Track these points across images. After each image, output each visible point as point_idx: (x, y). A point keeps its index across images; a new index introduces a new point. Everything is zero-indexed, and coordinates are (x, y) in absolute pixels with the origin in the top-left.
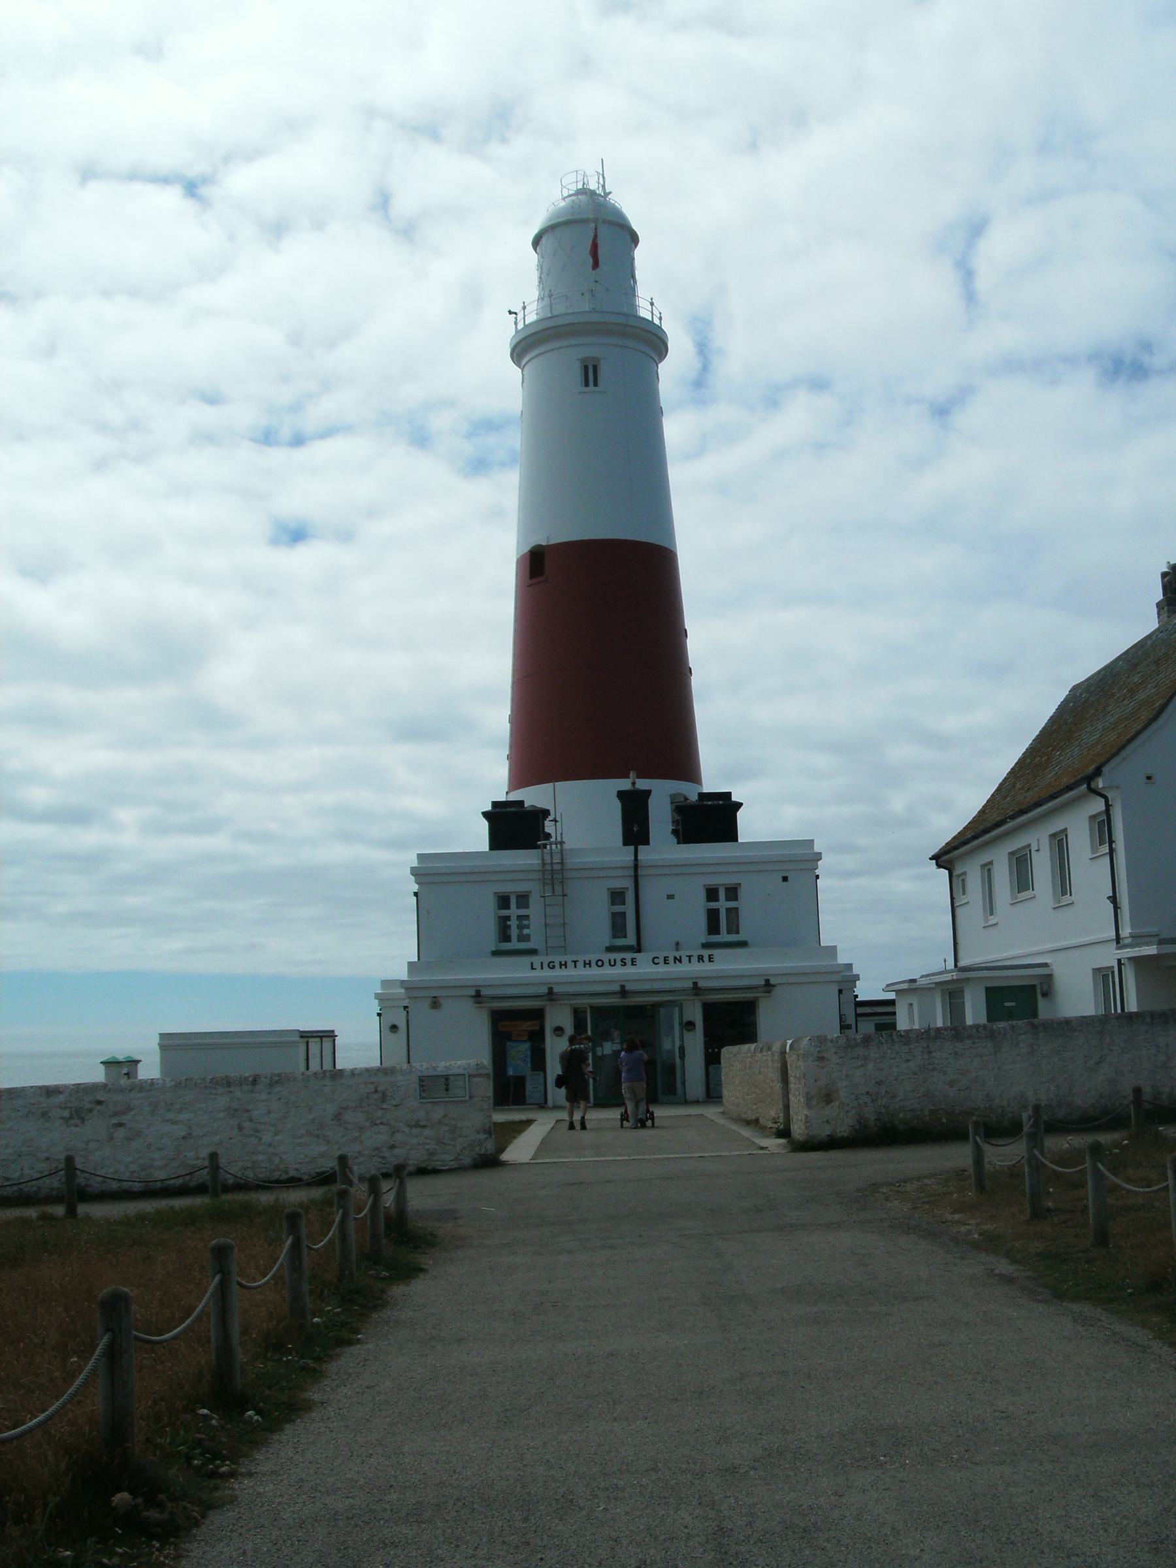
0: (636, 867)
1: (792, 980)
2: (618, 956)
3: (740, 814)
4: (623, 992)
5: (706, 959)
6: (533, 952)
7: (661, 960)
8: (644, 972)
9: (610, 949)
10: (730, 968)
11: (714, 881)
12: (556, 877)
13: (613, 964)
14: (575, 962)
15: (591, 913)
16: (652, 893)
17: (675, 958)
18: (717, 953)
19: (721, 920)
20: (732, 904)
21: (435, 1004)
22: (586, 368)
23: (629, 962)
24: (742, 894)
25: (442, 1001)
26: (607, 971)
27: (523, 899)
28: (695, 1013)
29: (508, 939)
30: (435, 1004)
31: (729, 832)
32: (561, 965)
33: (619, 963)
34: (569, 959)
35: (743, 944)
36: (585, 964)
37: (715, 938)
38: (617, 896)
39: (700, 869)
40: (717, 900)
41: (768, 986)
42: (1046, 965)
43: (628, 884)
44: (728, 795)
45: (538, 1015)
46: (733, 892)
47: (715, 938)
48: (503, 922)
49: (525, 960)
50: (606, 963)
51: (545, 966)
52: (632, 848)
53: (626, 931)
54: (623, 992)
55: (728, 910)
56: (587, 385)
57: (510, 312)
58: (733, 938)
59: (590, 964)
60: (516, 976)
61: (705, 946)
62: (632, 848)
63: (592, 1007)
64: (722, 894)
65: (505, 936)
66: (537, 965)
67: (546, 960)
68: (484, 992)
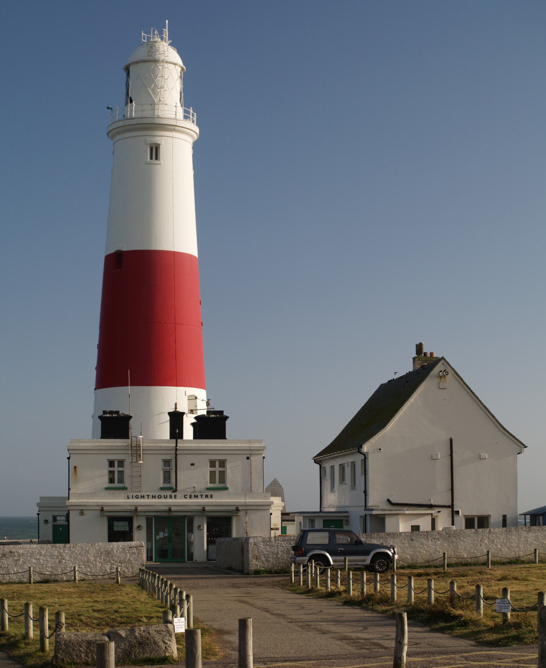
0: (176, 450)
1: (258, 508)
2: (163, 493)
3: (228, 422)
4: (170, 510)
5: (209, 496)
6: (125, 489)
7: (188, 497)
8: (179, 502)
9: (162, 489)
10: (220, 500)
11: (112, 457)
12: (136, 451)
13: (166, 497)
14: (148, 496)
15: (152, 470)
16: (183, 461)
17: (195, 496)
18: (214, 493)
19: (219, 480)
20: (121, 469)
21: (82, 513)
22: (151, 149)
23: (173, 496)
24: (228, 465)
25: (85, 512)
26: (163, 500)
27: (121, 463)
28: (143, 522)
29: (116, 479)
30: (82, 513)
31: (221, 434)
32: (141, 497)
33: (168, 497)
34: (145, 494)
35: (226, 489)
36: (153, 497)
37: (112, 485)
38: (167, 463)
39: (203, 452)
40: (215, 467)
41: (237, 510)
42: (347, 512)
43: (172, 457)
44: (221, 412)
45: (130, 520)
46: (223, 463)
47: (112, 485)
48: (212, 474)
49: (122, 493)
50: (163, 497)
51: (134, 497)
52: (174, 440)
53: (170, 484)
54: (170, 510)
55: (119, 471)
56: (151, 158)
57: (108, 108)
58: (121, 485)
59: (155, 497)
60: (119, 501)
61: (162, 489)
62: (174, 440)
63: (155, 516)
64: (116, 464)
65: (111, 481)
66: (130, 497)
67: (135, 494)
68: (105, 508)
